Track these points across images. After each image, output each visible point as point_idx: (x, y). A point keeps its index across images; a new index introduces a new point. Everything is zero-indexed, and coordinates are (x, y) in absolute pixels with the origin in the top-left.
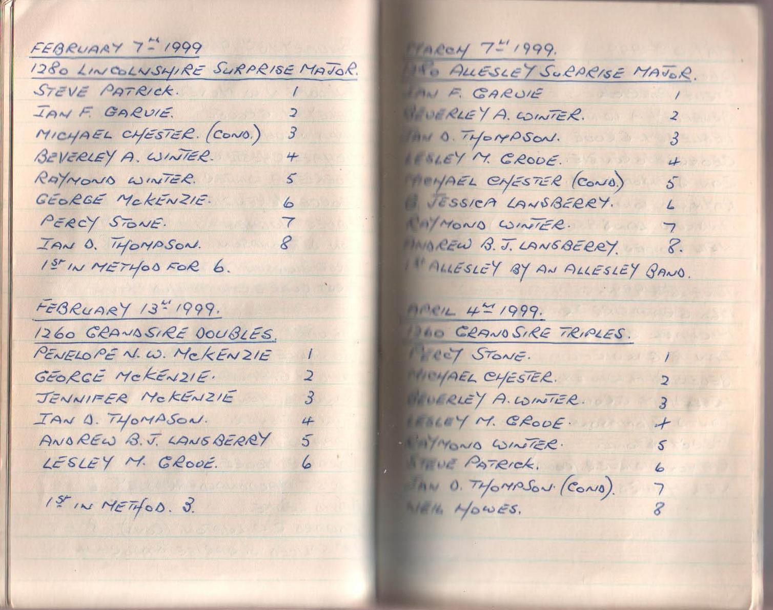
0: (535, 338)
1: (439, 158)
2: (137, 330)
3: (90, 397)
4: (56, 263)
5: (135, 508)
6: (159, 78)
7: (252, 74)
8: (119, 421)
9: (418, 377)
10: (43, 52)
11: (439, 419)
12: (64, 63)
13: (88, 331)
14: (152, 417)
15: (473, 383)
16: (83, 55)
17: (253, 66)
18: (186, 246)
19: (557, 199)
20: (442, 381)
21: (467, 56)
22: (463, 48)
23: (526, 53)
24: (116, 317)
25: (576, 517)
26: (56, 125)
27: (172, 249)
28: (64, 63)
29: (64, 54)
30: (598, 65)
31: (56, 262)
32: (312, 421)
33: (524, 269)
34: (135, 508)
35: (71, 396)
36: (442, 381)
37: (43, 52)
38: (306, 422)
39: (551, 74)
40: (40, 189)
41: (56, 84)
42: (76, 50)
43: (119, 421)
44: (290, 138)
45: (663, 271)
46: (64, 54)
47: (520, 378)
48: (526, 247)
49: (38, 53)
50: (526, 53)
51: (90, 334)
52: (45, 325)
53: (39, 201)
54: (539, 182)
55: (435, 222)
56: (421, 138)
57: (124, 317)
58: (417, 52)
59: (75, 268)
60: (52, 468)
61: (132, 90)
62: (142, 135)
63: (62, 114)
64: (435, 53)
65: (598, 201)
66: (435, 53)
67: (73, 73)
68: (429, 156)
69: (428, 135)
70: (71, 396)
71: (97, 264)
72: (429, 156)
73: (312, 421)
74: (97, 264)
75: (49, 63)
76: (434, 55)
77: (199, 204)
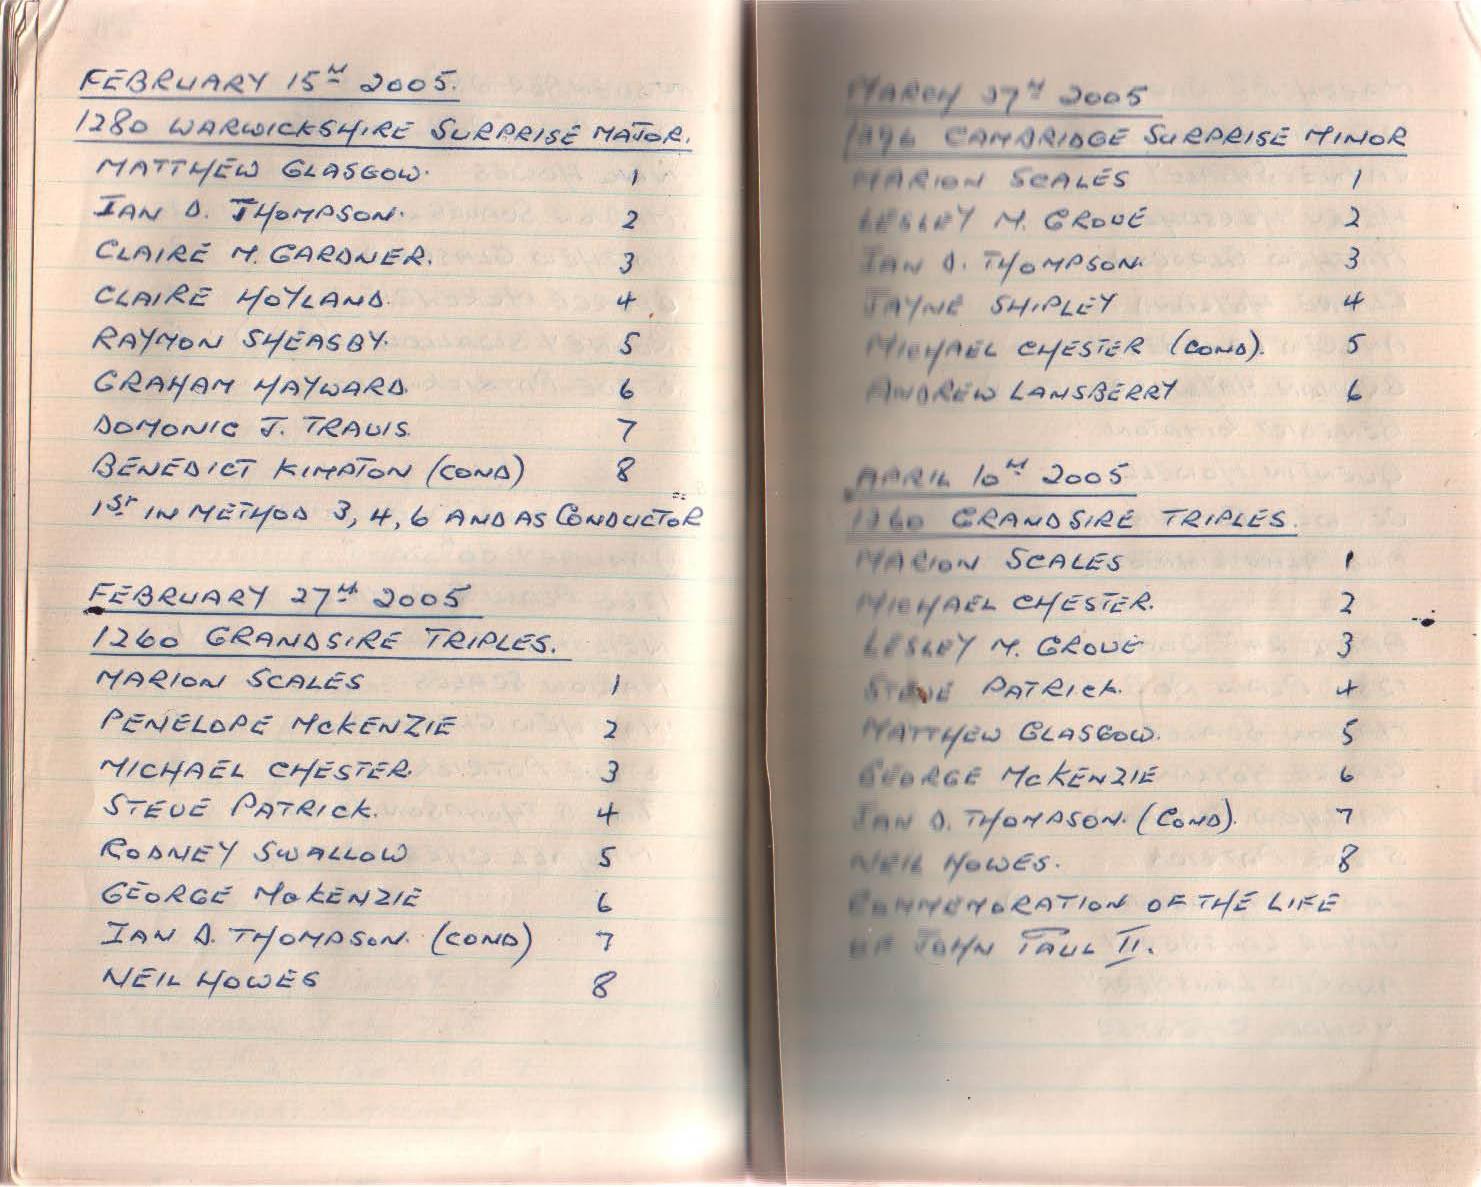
0: (169, 606)
1: (929, 644)
2: (313, 636)
3: (136, 764)
4: (117, 505)
5: (1216, 905)
6: (1384, 152)
7: (1253, 147)
8: (258, 214)
9: (889, 347)
10: (106, 87)
11: (929, 644)
12: (141, 111)
13: (211, 632)
14: (1023, 768)
15: (991, 611)
16: (186, 93)
17: (1401, 128)
18: (357, 260)
19: (1024, 608)
20: (951, 745)
21: (958, 104)
22: (180, 381)
23: (257, 89)
24: (240, 609)
25: (497, 1045)
26: (130, 234)
27: (1086, 474)
28: (141, 111)
29: (148, 93)
30: (237, 116)
31: (119, 502)
32: (616, 813)
33: (375, 343)
34: (1216, 905)
35: (284, 334)
36: (951, 745)
37: (106, 87)
38: (604, 815)
39: (448, 135)
40: (101, 361)
41: (133, 154)
42: (171, 84)
43: (258, 214)
44: (624, 272)
45: (1060, 559)
46: (148, 93)
47: (341, 770)
48: (190, 599)
49: (90, 89)
50: (257, 89)
51: (213, 639)
52: (97, 107)
53: (101, 385)
54: (665, 521)
55: (916, 308)
56: (892, 824)
57: (259, 610)
58: (867, 98)
59: (160, 514)
60: (652, 513)
61: (181, 166)
62: (270, 214)
63: (173, 852)
64: (902, 98)
65: (247, 79)
66: (902, 98)
67: (159, 130)
68: (904, 219)
69: (906, 819)
70: (284, 334)
71: (198, 508)
72: (904, 219)
73: (616, 813)
74: (198, 508)
75: (109, 109)
76: (899, 102)
77: (218, 902)
